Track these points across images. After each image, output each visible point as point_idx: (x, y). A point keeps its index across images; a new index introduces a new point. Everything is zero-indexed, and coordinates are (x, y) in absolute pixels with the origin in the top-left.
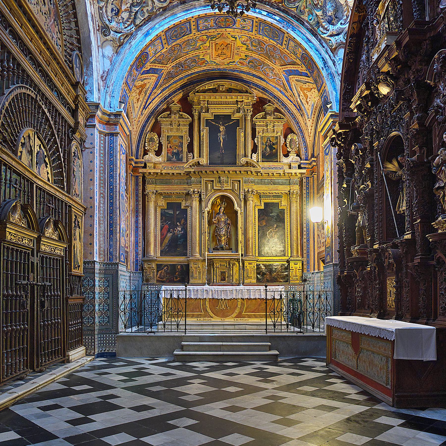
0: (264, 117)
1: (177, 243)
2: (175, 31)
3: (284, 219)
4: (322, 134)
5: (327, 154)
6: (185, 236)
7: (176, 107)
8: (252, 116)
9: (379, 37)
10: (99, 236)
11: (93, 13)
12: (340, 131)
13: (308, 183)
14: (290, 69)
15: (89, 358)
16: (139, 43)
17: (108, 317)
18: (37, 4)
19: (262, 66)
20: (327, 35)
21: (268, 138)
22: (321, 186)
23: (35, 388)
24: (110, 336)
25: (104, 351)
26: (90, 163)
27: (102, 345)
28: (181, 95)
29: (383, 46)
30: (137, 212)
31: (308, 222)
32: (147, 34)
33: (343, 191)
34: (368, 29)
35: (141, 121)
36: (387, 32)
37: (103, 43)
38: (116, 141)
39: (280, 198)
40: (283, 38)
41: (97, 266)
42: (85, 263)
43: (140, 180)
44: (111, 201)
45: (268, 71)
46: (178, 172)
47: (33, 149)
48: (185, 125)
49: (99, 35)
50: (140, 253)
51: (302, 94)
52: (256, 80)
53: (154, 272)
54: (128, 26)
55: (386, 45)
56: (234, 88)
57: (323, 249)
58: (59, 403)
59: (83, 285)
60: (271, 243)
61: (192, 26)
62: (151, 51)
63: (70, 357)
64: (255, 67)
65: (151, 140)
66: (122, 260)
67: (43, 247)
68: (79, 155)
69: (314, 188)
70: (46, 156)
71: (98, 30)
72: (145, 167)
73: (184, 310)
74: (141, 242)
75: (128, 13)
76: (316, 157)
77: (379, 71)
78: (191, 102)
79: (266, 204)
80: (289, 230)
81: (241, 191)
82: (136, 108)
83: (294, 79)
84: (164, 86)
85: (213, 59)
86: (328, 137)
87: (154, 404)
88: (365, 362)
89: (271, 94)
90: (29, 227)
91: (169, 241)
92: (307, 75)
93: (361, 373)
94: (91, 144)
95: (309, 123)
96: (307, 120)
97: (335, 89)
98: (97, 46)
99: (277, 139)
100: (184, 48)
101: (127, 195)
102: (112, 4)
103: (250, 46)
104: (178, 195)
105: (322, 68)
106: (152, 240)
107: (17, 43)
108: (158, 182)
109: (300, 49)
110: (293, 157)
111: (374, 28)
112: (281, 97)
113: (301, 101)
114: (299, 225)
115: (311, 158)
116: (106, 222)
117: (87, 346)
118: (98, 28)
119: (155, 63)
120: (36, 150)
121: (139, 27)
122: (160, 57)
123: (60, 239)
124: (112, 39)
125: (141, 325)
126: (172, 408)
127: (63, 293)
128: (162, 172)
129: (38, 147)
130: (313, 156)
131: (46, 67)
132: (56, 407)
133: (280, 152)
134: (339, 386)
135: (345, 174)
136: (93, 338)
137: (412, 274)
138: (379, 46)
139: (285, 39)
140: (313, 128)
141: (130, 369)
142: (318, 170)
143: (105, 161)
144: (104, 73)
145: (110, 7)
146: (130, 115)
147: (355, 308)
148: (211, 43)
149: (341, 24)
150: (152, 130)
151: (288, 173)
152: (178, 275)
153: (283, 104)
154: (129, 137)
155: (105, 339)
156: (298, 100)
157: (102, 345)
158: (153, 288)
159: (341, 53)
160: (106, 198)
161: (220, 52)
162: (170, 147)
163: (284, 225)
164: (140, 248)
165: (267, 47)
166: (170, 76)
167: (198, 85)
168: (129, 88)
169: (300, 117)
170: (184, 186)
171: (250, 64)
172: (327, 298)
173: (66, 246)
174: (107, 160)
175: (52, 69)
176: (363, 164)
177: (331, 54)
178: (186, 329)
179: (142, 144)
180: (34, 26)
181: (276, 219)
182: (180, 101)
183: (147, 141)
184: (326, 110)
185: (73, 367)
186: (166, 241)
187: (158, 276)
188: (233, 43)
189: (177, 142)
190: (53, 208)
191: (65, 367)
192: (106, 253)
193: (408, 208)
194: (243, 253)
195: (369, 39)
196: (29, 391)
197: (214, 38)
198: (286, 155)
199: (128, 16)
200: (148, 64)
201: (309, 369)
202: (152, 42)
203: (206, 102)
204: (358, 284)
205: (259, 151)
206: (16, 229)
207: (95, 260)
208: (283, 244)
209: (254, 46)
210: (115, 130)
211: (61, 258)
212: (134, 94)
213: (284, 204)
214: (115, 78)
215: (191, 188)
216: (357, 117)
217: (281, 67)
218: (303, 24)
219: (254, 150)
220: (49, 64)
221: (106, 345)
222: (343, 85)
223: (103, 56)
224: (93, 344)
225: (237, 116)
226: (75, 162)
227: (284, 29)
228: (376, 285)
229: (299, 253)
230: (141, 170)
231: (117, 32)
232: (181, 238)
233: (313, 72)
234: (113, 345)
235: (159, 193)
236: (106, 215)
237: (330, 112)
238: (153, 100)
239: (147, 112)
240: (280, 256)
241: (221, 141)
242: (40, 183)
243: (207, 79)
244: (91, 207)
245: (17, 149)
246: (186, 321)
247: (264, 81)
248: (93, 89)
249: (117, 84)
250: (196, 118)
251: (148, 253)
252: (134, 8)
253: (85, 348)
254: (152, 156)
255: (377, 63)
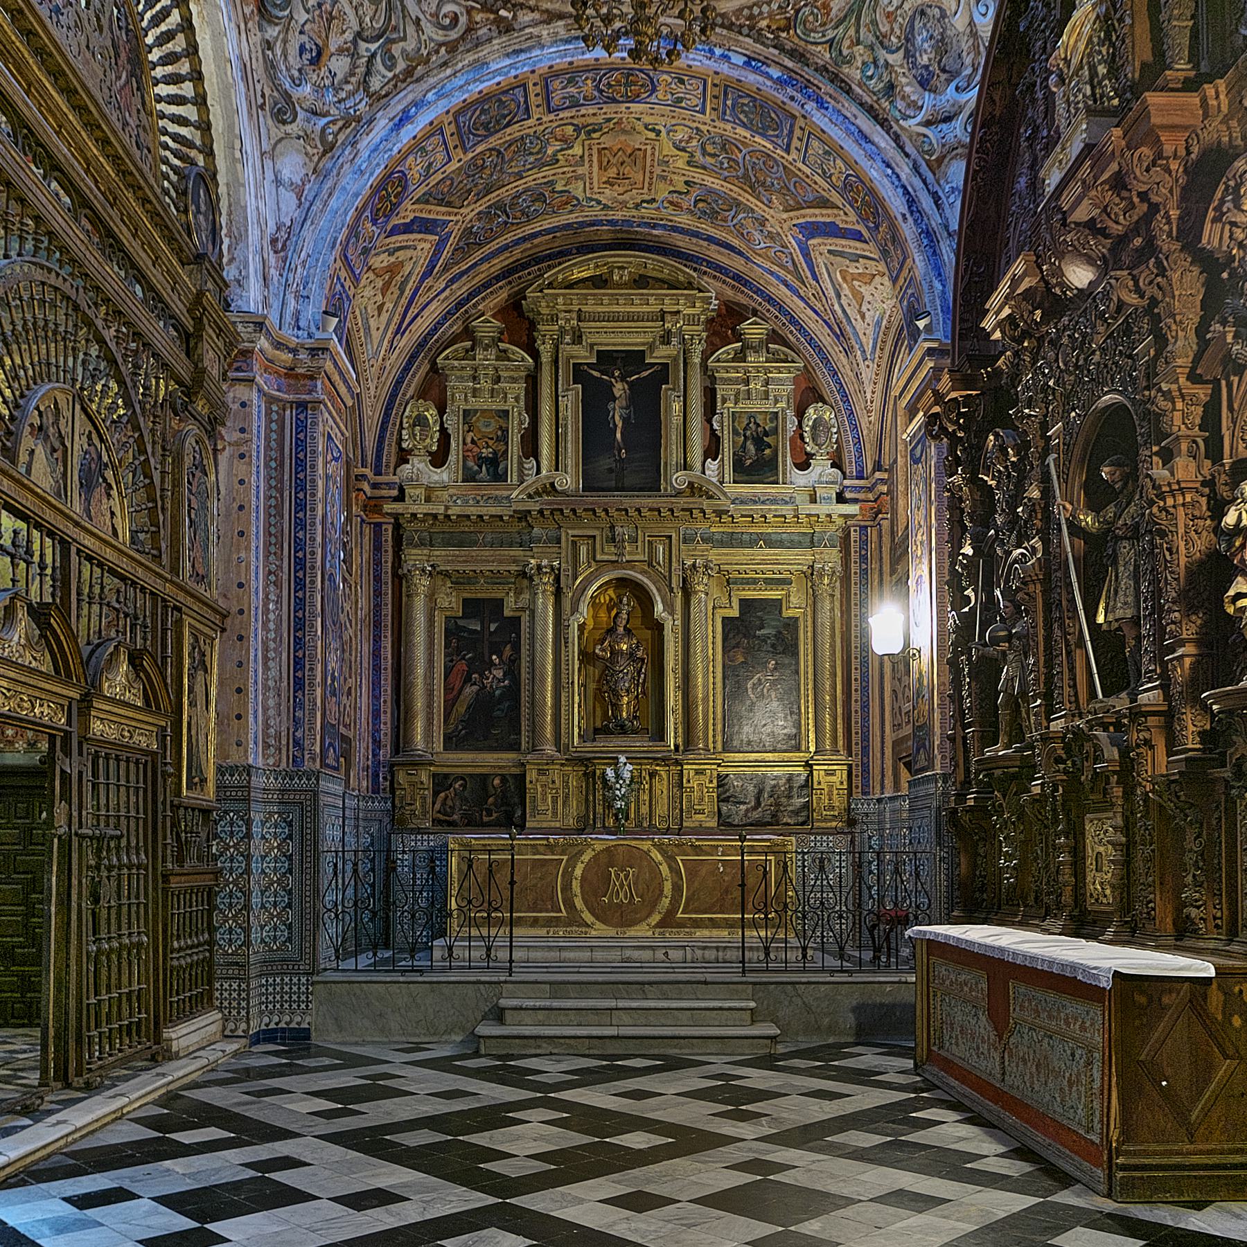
0: (740, 356)
1: (493, 716)
2: (483, 111)
3: (796, 646)
4: (903, 403)
5: (916, 461)
6: (513, 693)
7: (488, 326)
8: (705, 357)
9: (1064, 123)
10: (264, 694)
11: (247, 58)
12: (953, 395)
13: (864, 543)
14: (813, 219)
15: (232, 1047)
16: (377, 146)
17: (290, 927)
18: (76, 26)
19: (732, 213)
20: (918, 119)
21: (751, 416)
22: (900, 554)
23: (62, 1138)
24: (295, 980)
25: (277, 1024)
26: (237, 486)
27: (270, 1006)
28: (504, 295)
29: (1075, 148)
30: (377, 625)
31: (864, 654)
32: (404, 119)
33: (964, 567)
34: (1033, 101)
35: (388, 368)
36: (1087, 107)
37: (276, 144)
38: (315, 424)
39: (785, 587)
40: (791, 132)
41: (258, 781)
42: (220, 770)
43: (392, 537)
44: (300, 594)
45: (750, 226)
46: (494, 511)
47: (68, 445)
48: (514, 380)
49: (267, 121)
50: (386, 740)
51: (846, 290)
52: (715, 253)
53: (424, 798)
54: (348, 97)
55: (1087, 145)
56: (655, 274)
57: (907, 730)
58: (127, 1185)
59: (216, 836)
60: (759, 715)
61: (532, 95)
62: (414, 167)
63: (175, 1043)
64: (713, 215)
65: (420, 421)
66: (330, 761)
67: (97, 727)
68: (205, 462)
69: (881, 559)
70: (106, 465)
71: (262, 107)
72: (401, 498)
73: (507, 904)
74: (389, 711)
75: (349, 59)
76: (886, 470)
77: (1064, 219)
78: (531, 315)
79: (743, 602)
80: (810, 676)
81: (674, 565)
82: (374, 332)
83: (824, 249)
84: (456, 270)
85: (594, 194)
86: (921, 413)
87: (405, 1185)
88: (1025, 1061)
89: (758, 291)
90: (57, 671)
91: (468, 708)
92: (858, 237)
93: (1014, 1093)
94: (242, 430)
95: (867, 374)
96: (862, 366)
97: (940, 275)
98: (257, 154)
99: (777, 418)
100: (511, 160)
101: (347, 576)
102: (301, 32)
103: (698, 155)
104: (496, 578)
105: (904, 215)
106: (419, 704)
107: (15, 136)
108: (438, 539)
109: (839, 162)
110: (821, 469)
111: (1049, 97)
112: (788, 301)
113: (844, 311)
114: (839, 662)
115: (874, 471)
116: (285, 655)
117: (226, 1012)
118: (260, 101)
119: (427, 202)
120: (76, 447)
121: (380, 99)
122: (441, 187)
123: (151, 703)
124: (301, 133)
125: (387, 946)
126: (459, 1199)
127: (155, 858)
128: (450, 512)
129: (85, 438)
130: (878, 467)
131: (105, 210)
132: (119, 1195)
133: (784, 456)
134: (952, 1131)
135: (969, 516)
136: (243, 986)
137: (1161, 806)
138: (1063, 149)
139: (797, 133)
140: (880, 386)
141: (347, 1079)
142: (892, 508)
143: (281, 481)
144: (278, 229)
145: (295, 41)
146: (357, 350)
147: (1000, 900)
148: (586, 147)
149: (957, 88)
150: (422, 394)
151: (808, 516)
152: (495, 804)
153: (793, 321)
154: (354, 413)
155: (278, 989)
156: (837, 307)
157: (270, 1006)
158: (426, 843)
159: (957, 171)
160: (285, 585)
161: (612, 172)
162: (473, 442)
163: (798, 663)
164: (386, 729)
165: (748, 157)
166: (471, 239)
167: (550, 267)
168: (353, 272)
169: (842, 356)
170: (512, 553)
171: (701, 205)
172: (918, 875)
173: (164, 724)
174: (286, 477)
175: (122, 214)
176: (1020, 487)
177: (929, 176)
178: (511, 961)
179: (392, 433)
180: (69, 92)
181: (773, 646)
182: (501, 313)
183: (405, 425)
184: (915, 334)
185: (181, 1073)
186: (461, 708)
187: (437, 806)
188: (649, 147)
189: (492, 428)
190: (126, 615)
191: (158, 1075)
192: (284, 742)
193: (1150, 614)
194: (680, 740)
195: (1036, 129)
196: (44, 1147)
197: (595, 131)
198: (803, 466)
199: (347, 69)
200: (407, 204)
201: (864, 1077)
202: (418, 146)
203: (575, 315)
204: (1006, 832)
205: (726, 454)
206: (12, 675)
207: (251, 761)
208: (795, 717)
209: (710, 155)
210: (310, 392)
211: (149, 758)
212: (368, 292)
213: (796, 606)
214: (312, 244)
215: (533, 557)
216: (1002, 353)
217: (785, 216)
218: (848, 91)
219: (712, 451)
220: (115, 199)
221: (282, 1006)
222: (962, 262)
223: (278, 182)
224: (244, 1004)
225: (662, 353)
226: (195, 484)
227: (794, 107)
228: (1058, 836)
229: (840, 743)
230: (388, 507)
231: (315, 113)
232: (500, 700)
233: (877, 227)
234: (303, 1006)
235: (440, 573)
236: (285, 635)
237: (925, 340)
238: (423, 309)
239: (406, 343)
240: (785, 751)
241: (615, 426)
242: (89, 541)
243: (577, 249)
244: (241, 612)
245: (17, 443)
246: (511, 937)
247: (740, 253)
248: (248, 277)
249: (317, 260)
250: (545, 358)
251: (409, 740)
252: (363, 45)
253: (220, 1015)
254: (421, 466)
255: (1058, 198)
